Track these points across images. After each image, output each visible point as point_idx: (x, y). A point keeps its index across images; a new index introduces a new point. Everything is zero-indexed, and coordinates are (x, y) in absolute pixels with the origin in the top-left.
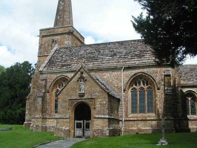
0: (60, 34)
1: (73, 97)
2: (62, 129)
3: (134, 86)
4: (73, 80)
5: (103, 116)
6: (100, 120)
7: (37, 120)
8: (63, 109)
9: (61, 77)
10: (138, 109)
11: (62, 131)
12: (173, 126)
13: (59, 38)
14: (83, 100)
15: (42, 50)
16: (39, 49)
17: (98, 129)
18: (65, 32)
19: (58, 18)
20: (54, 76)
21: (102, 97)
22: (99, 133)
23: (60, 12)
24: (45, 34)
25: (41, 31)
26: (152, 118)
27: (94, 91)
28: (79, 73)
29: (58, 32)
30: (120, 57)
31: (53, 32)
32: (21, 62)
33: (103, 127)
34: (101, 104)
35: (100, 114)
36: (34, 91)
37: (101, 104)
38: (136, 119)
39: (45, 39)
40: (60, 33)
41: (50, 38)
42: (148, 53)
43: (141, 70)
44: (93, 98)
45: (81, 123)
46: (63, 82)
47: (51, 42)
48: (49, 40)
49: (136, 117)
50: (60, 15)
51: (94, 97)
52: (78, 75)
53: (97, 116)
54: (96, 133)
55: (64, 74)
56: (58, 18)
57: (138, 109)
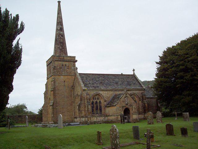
14: (128, 107)
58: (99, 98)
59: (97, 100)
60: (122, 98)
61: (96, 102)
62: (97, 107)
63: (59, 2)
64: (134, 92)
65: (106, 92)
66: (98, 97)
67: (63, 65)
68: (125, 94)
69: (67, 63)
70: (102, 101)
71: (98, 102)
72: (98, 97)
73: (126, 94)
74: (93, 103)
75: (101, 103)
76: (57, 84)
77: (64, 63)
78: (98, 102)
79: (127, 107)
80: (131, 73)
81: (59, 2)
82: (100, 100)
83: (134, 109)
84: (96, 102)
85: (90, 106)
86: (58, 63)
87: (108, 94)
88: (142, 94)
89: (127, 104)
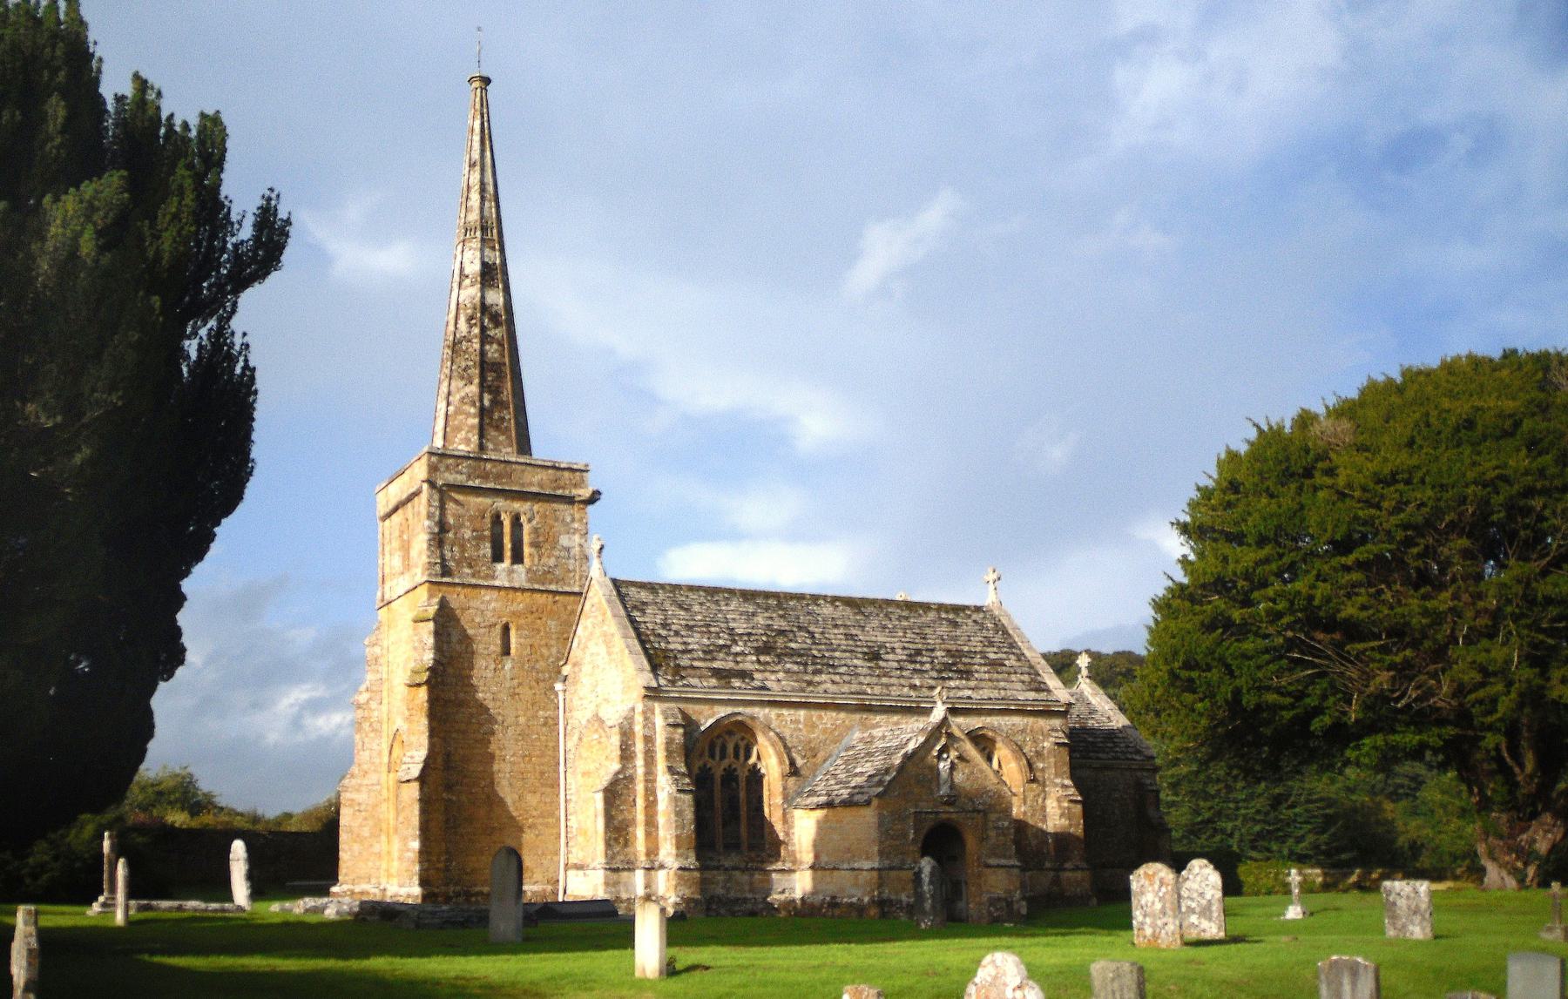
1: (922, 804)
5: (1003, 862)
11: (901, 909)
14: (954, 816)
18: (559, 492)
19: (487, 403)
25: (434, 459)
29: (531, 484)
31: (498, 477)
40: (534, 489)
53: (992, 861)
56: (487, 403)
66: (742, 744)
72: (742, 744)
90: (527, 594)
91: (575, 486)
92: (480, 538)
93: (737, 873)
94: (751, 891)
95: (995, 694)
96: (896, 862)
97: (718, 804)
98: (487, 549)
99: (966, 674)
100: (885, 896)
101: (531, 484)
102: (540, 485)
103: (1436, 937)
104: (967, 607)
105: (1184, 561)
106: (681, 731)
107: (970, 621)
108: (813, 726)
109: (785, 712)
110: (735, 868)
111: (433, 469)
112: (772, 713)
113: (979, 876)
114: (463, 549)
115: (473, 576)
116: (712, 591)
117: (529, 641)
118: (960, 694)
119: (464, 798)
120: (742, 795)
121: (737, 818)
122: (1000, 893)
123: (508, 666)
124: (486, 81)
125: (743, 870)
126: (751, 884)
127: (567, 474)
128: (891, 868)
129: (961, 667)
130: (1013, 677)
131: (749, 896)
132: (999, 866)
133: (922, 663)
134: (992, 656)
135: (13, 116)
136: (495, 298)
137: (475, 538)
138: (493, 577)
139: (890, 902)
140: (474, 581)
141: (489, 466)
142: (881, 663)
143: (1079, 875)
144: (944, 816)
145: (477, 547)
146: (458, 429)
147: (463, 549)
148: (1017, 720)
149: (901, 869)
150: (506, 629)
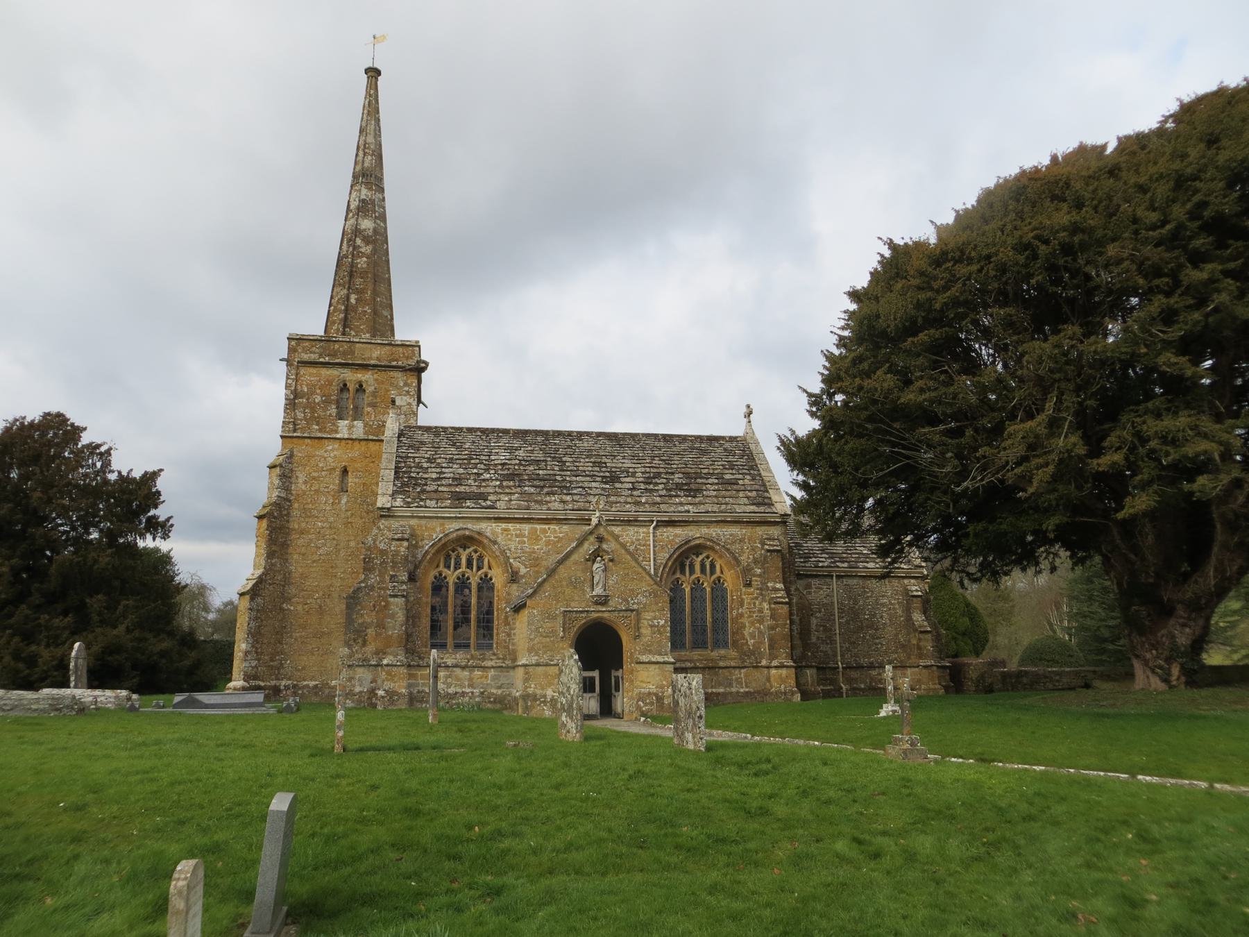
0: (375, 366)
1: (573, 604)
2: (545, 696)
3: (678, 575)
4: (575, 557)
5: (660, 659)
6: (653, 666)
7: (389, 673)
8: (544, 640)
9: (459, 533)
10: (688, 637)
11: (544, 702)
12: (793, 682)
13: (371, 381)
14: (606, 615)
15: (300, 415)
16: (286, 409)
17: (650, 693)
18: (394, 363)
19: (353, 301)
20: (434, 529)
21: (654, 607)
22: (652, 704)
23: (358, 281)
24: (314, 357)
25: (293, 343)
26: (733, 664)
27: (632, 590)
28: (592, 539)
29: (371, 358)
30: (634, 489)
31: (344, 354)
32: (33, 414)
33: (662, 687)
34: (651, 626)
35: (650, 652)
36: (272, 565)
37: (651, 626)
38: (688, 665)
39: (309, 375)
40: (373, 362)
41: (334, 372)
42: (710, 481)
43: (704, 530)
44: (632, 611)
45: (593, 679)
46: (461, 550)
47: (335, 389)
48: (330, 382)
49: (690, 661)
50: (358, 292)
51: (635, 607)
52: (589, 547)
53: (644, 658)
54: (646, 704)
55: (470, 526)
56: (353, 301)
57: (688, 637)
58: (713, 566)
59: (469, 573)
60: (568, 563)
61: (462, 584)
62: (465, 609)
63: (373, 73)
64: (714, 531)
65: (526, 527)
66: (475, 556)
67: (344, 388)
68: (592, 539)
69: (367, 377)
70: (498, 577)
71: (474, 582)
72: (475, 556)
73: (600, 539)
74: (439, 587)
75: (492, 588)
76: (300, 482)
77: (351, 376)
78: (474, 582)
79: (604, 613)
80: (732, 427)
81: (373, 73)
82: (485, 569)
83: (646, 631)
84: (462, 584)
85: (401, 601)
86: (319, 375)
87: (535, 538)
88: (763, 544)
89: (603, 601)
90: (363, 443)
91: (407, 358)
92: (327, 402)
93: (458, 671)
94: (471, 686)
95: (716, 508)
96: (545, 658)
97: (450, 609)
98: (333, 410)
99: (693, 492)
100: (530, 691)
101: (371, 358)
102: (378, 359)
103: (587, 738)
104: (723, 438)
105: (825, 367)
106: (405, 544)
107: (720, 450)
108: (537, 539)
109: (510, 526)
110: (456, 666)
111: (291, 350)
112: (498, 527)
113: (632, 672)
114: (313, 410)
115: (320, 430)
116: (485, 432)
117: (362, 481)
118: (681, 508)
119: (300, 608)
120: (474, 600)
121: (468, 621)
122: (653, 689)
123: (344, 500)
124: (378, 72)
125: (463, 668)
126: (471, 679)
127: (401, 349)
128: (538, 665)
129: (693, 486)
130: (741, 494)
131: (468, 690)
132: (650, 663)
133: (657, 484)
134: (727, 477)
135: (1134, 371)
136: (367, 224)
137: (323, 402)
138: (337, 432)
139: (534, 697)
140: (319, 435)
141: (337, 346)
142: (618, 485)
143: (784, 672)
144: (595, 615)
145: (325, 409)
146: (334, 323)
147: (313, 410)
148: (735, 530)
149: (547, 665)
150: (345, 471)
